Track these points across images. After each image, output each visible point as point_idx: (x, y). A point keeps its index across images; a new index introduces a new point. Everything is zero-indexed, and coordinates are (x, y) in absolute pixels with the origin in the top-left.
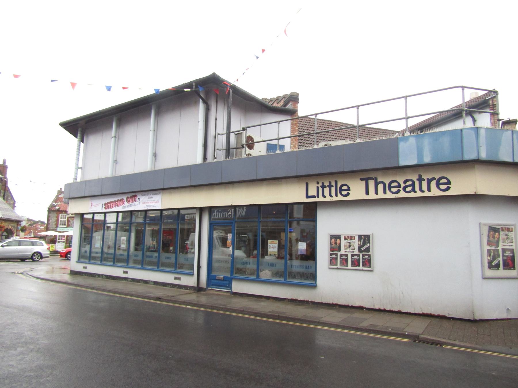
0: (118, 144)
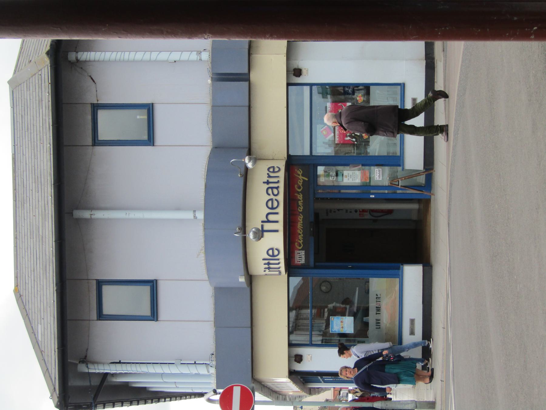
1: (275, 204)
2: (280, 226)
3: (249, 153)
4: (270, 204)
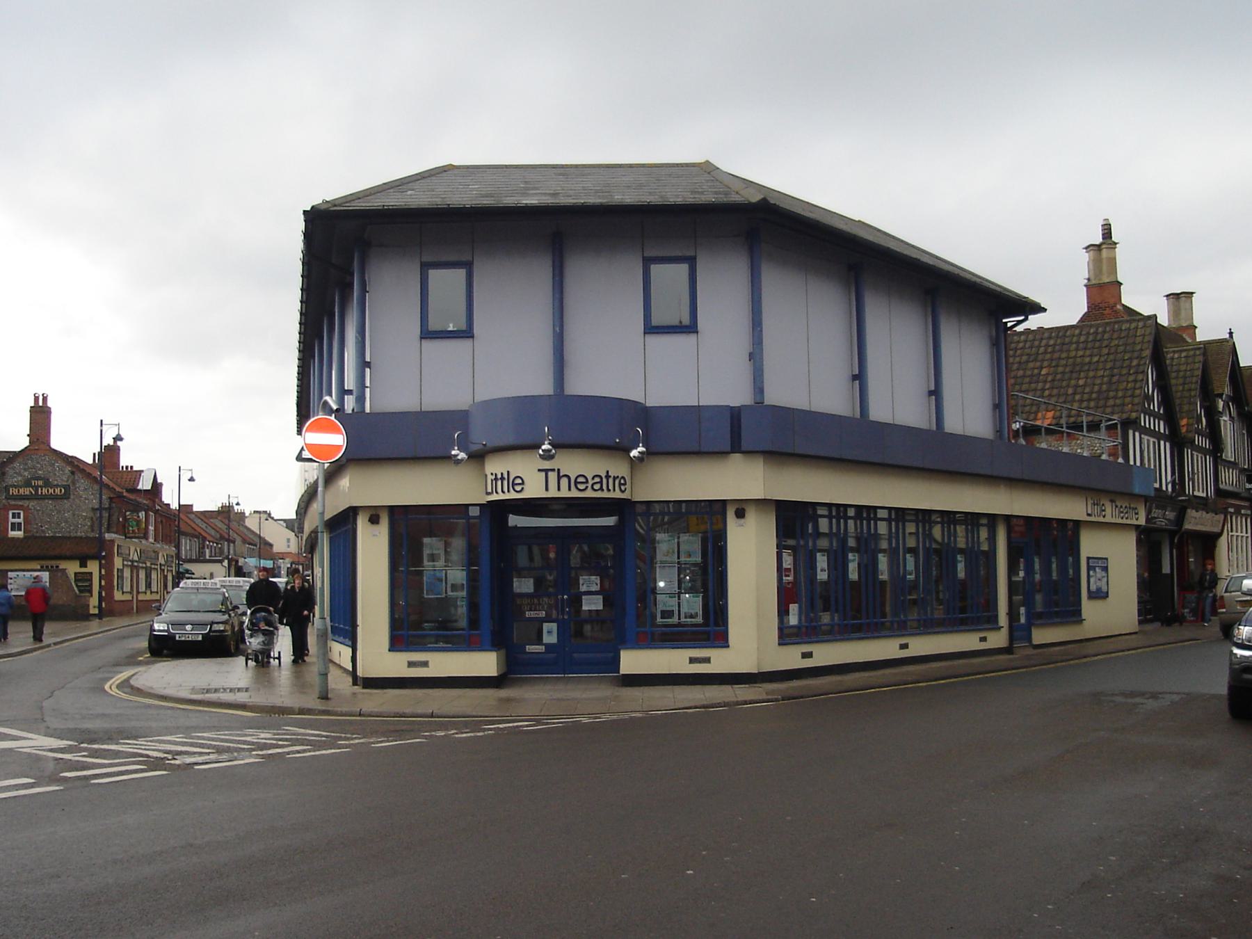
0: (364, 290)
1: (581, 487)
2: (553, 493)
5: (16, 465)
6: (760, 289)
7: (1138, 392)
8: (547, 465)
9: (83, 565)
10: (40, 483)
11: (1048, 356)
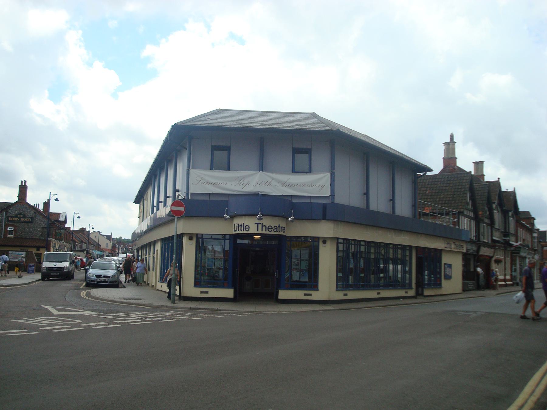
1: (270, 230)
3: (295, 219)
4: (270, 227)
5: (12, 208)
6: (334, 161)
7: (464, 201)
8: (258, 222)
9: (38, 250)
10: (22, 216)
11: (429, 186)
